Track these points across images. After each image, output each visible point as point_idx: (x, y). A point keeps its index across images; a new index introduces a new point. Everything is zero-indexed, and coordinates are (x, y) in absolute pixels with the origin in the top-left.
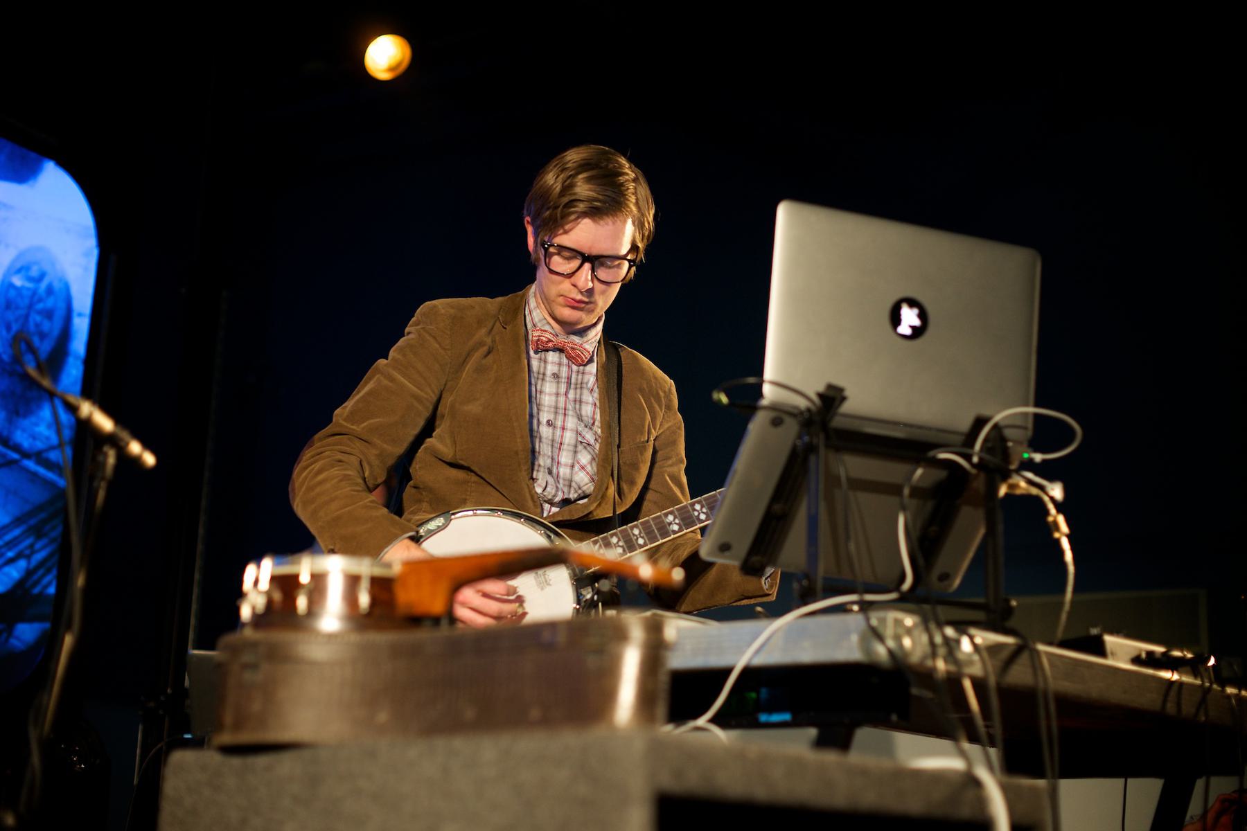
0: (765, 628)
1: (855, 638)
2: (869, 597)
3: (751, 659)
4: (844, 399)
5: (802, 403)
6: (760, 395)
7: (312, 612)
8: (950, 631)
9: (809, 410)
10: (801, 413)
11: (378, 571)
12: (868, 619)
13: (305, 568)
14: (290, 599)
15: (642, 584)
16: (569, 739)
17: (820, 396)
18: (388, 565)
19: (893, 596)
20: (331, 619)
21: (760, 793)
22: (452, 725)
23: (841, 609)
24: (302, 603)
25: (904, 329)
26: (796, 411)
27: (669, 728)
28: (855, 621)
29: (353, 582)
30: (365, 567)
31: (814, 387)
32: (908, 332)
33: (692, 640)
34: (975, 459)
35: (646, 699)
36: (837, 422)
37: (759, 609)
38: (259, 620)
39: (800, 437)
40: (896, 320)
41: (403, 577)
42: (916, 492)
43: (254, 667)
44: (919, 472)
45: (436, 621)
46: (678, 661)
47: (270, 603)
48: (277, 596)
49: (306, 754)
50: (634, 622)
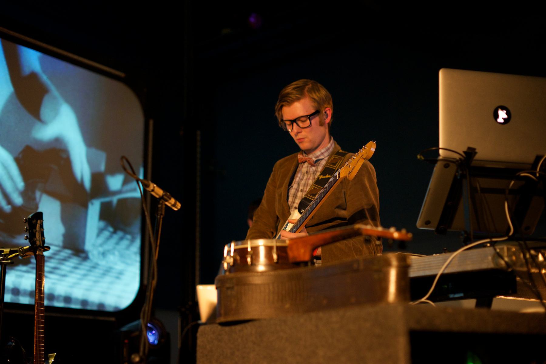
0: (450, 256)
1: (490, 258)
2: (494, 240)
3: (444, 270)
4: (476, 153)
5: (457, 156)
6: (439, 155)
7: (253, 264)
8: (532, 252)
9: (460, 159)
10: (457, 161)
11: (279, 244)
12: (495, 250)
13: (249, 245)
14: (244, 258)
15: (394, 240)
16: (369, 310)
17: (464, 152)
18: (284, 241)
19: (506, 238)
20: (261, 267)
21: (455, 328)
22: (317, 307)
23: (483, 246)
24: (249, 260)
25: (500, 120)
26: (455, 160)
27: (411, 303)
28: (489, 250)
29: (269, 249)
30: (274, 243)
31: (462, 149)
32: (502, 121)
33: (422, 265)
34: (538, 175)
35: (37, 324)
36: (474, 163)
37: (489, 245)
38: (233, 268)
39: (457, 172)
40: (496, 116)
41: (291, 245)
42: (512, 191)
43: (231, 288)
44: (513, 182)
45: (305, 263)
46: (413, 273)
47: (235, 260)
48: (238, 258)
49: (256, 323)
50: (393, 258)
